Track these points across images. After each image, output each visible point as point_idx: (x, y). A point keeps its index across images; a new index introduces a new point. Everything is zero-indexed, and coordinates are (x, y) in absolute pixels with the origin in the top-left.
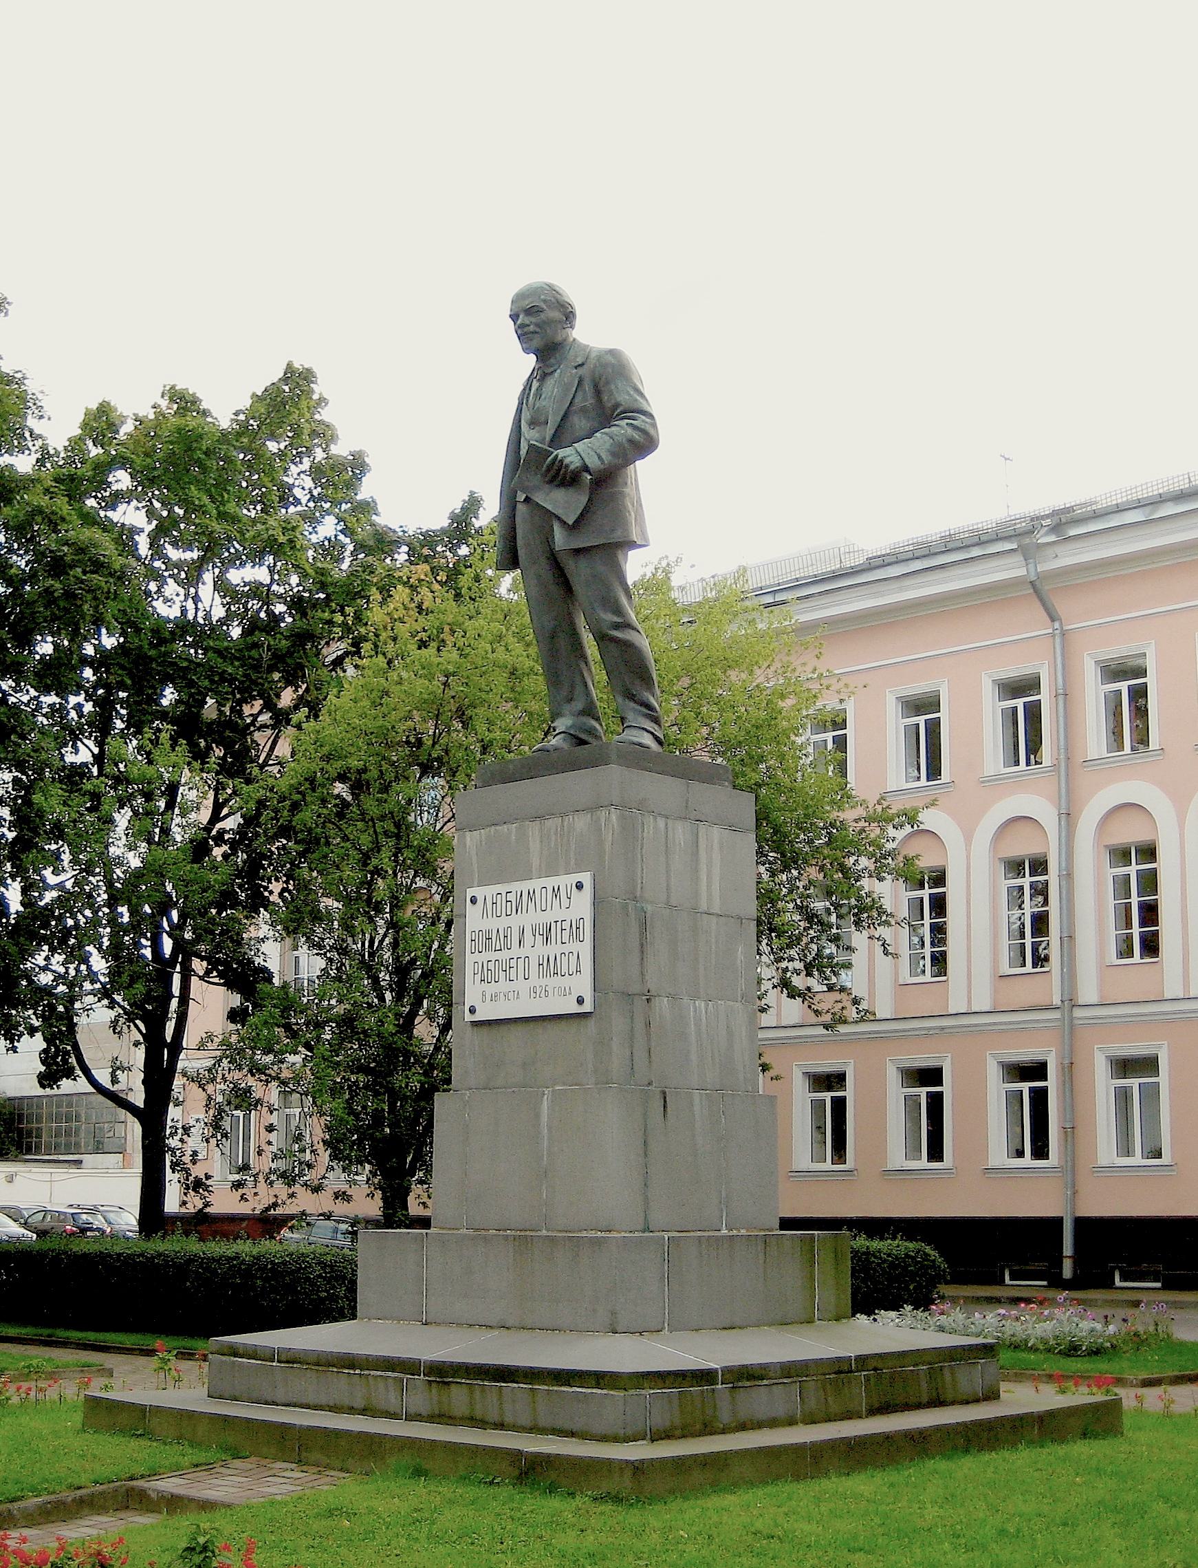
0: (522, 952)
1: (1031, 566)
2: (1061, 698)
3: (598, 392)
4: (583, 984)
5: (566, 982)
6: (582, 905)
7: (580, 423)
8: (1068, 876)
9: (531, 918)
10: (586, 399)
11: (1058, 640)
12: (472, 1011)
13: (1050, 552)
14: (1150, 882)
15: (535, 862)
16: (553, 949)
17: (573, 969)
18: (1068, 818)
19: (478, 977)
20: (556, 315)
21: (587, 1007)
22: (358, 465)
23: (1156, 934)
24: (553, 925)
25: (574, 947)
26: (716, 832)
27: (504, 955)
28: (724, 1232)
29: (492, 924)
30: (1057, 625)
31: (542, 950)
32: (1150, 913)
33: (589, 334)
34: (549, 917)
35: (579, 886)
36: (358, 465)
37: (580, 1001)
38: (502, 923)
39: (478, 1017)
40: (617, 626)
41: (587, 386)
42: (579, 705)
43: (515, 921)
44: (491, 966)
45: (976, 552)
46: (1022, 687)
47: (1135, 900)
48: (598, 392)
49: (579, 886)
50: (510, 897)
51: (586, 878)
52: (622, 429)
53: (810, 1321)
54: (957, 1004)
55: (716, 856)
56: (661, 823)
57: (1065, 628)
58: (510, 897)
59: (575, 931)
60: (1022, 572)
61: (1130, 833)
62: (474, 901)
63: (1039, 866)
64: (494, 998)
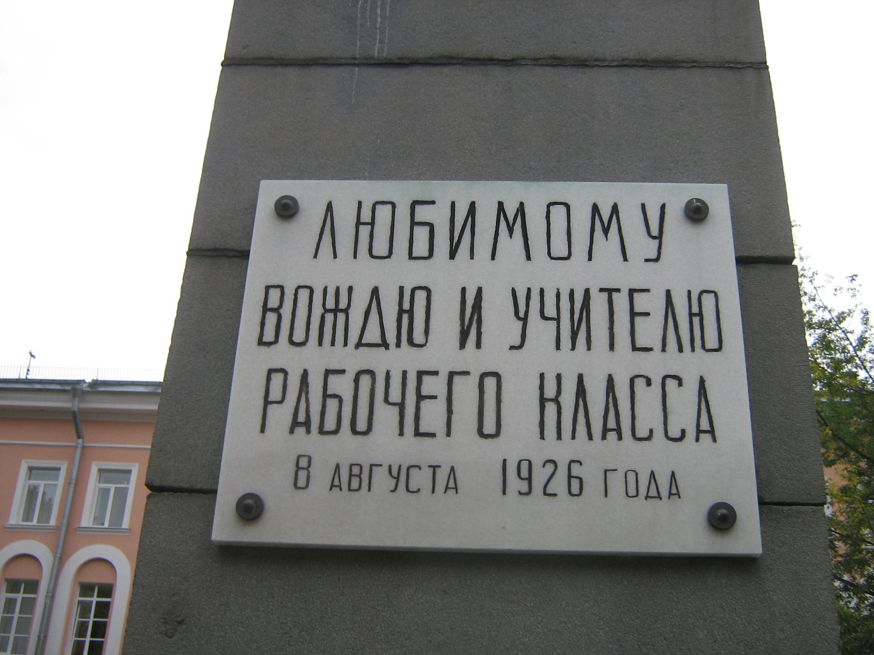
0: (474, 360)
1: (76, 403)
2: (72, 486)
8: (52, 596)
9: (500, 273)
11: (79, 451)
12: (250, 509)
14: (104, 610)
16: (598, 364)
17: (684, 413)
18: (60, 562)
19: (280, 415)
21: (748, 539)
23: (101, 644)
24: (599, 304)
25: (691, 365)
27: (399, 360)
29: (361, 275)
30: (80, 441)
31: (543, 352)
34: (575, 276)
37: (722, 519)
38: (395, 275)
39: (265, 533)
43: (447, 278)
44: (342, 386)
47: (92, 619)
50: (422, 213)
57: (87, 445)
58: (422, 213)
59: (686, 320)
61: (96, 576)
62: (286, 209)
63: (32, 586)
64: (353, 478)
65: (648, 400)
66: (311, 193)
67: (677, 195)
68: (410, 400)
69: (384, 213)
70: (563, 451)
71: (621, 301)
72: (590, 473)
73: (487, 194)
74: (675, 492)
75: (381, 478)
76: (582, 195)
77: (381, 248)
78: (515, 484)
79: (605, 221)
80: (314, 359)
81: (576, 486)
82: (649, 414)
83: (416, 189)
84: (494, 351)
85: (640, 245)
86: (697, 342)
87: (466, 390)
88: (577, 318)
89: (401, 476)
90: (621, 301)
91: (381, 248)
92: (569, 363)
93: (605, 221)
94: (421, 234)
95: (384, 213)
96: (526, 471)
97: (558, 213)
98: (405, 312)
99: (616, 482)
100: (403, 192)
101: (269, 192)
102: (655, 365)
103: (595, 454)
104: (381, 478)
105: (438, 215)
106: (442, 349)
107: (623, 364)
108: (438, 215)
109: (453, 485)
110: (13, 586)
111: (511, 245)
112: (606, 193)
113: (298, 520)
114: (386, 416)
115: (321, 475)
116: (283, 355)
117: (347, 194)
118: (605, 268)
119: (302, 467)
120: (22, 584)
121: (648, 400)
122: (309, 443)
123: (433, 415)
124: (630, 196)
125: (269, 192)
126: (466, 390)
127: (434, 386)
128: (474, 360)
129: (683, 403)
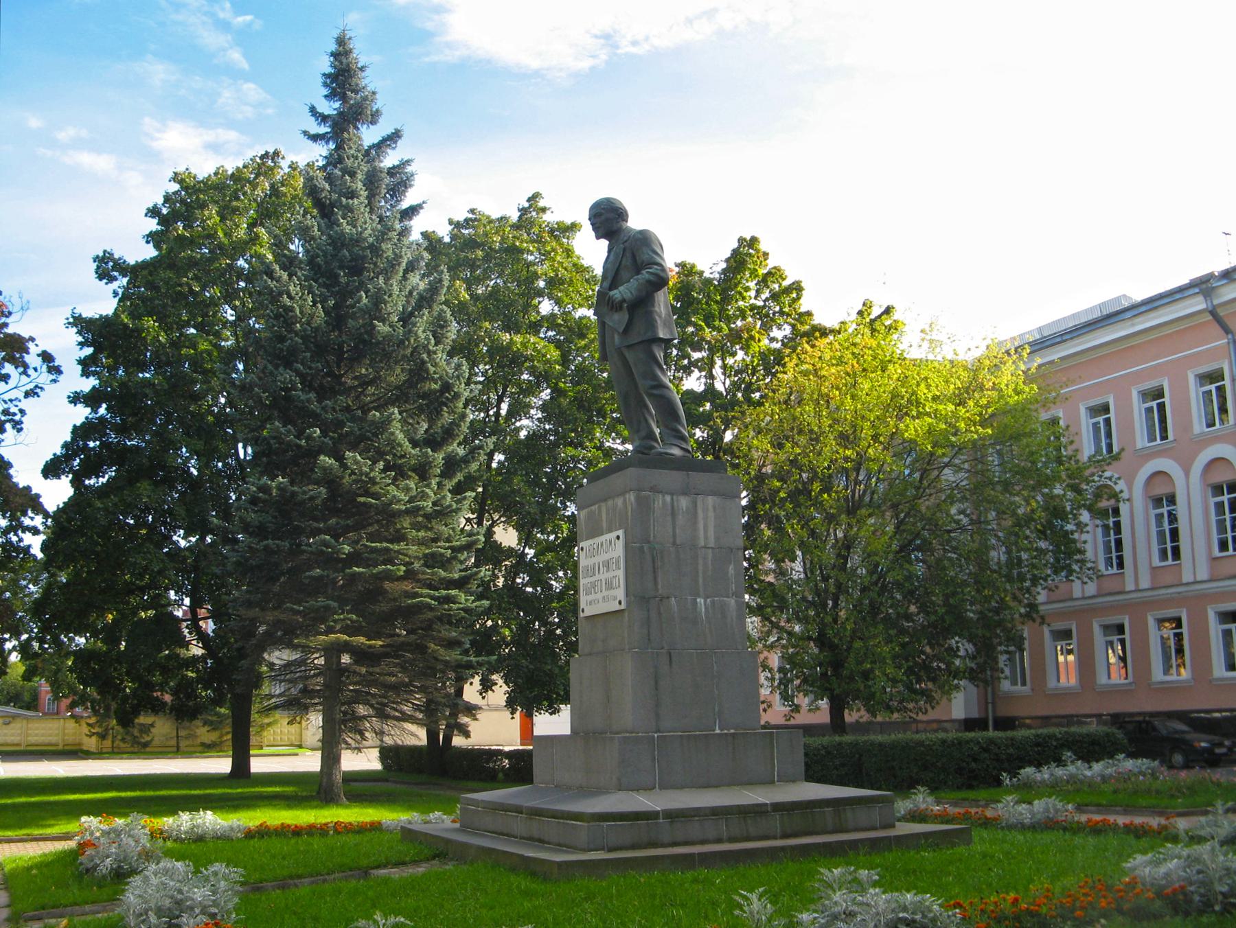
3: (634, 256)
4: (620, 593)
6: (618, 551)
7: (624, 274)
10: (627, 261)
13: (1223, 290)
15: (604, 525)
20: (611, 215)
22: (797, 287)
26: (710, 500)
28: (718, 731)
32: (1175, 534)
33: (635, 222)
35: (618, 538)
36: (797, 287)
40: (654, 387)
41: (628, 254)
42: (643, 433)
45: (1178, 296)
46: (1214, 377)
48: (634, 256)
49: (618, 538)
51: (620, 533)
52: (645, 275)
53: (773, 782)
54: (1187, 577)
55: (711, 514)
56: (668, 498)
60: (1203, 306)
67: (614, 535)
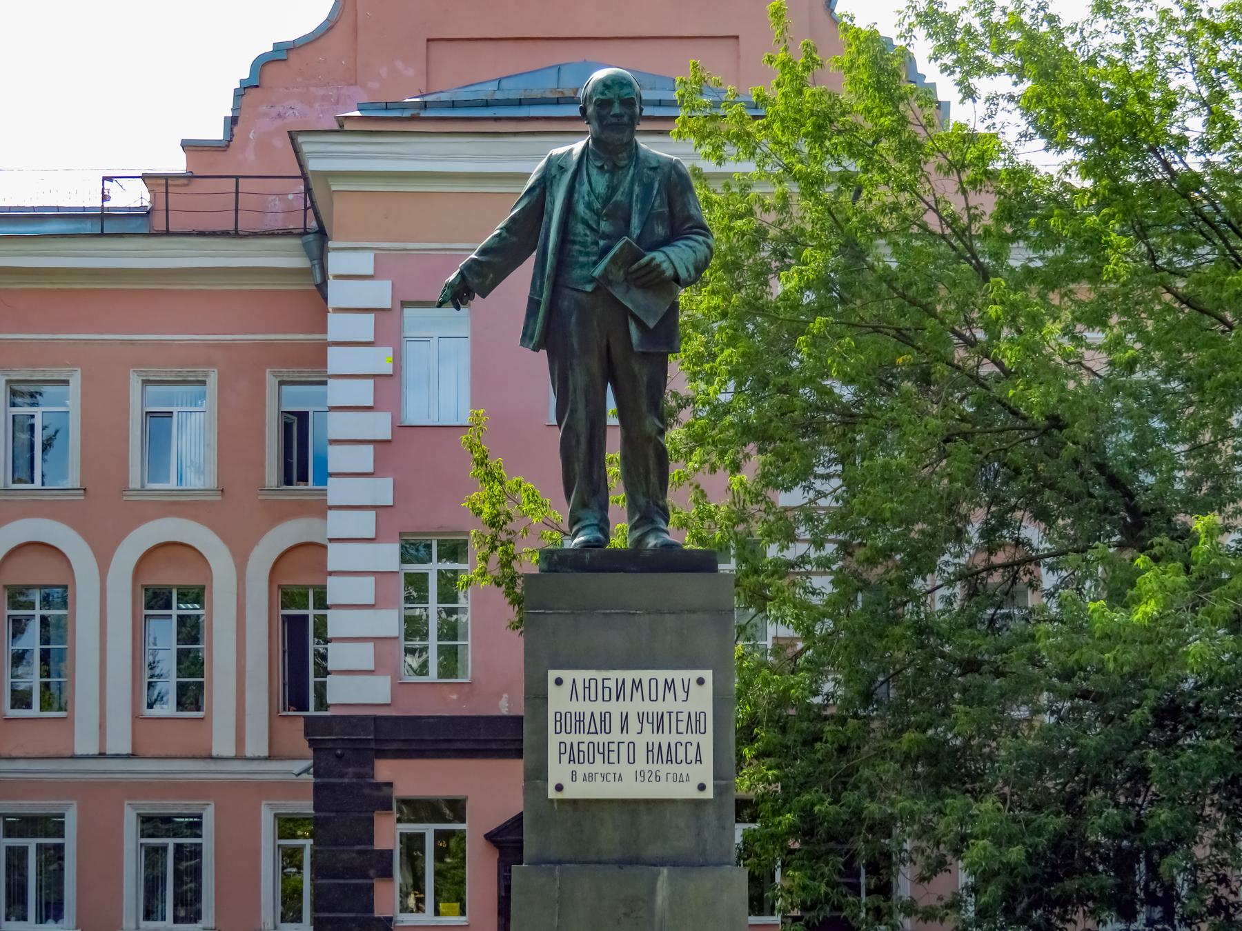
0: (626, 738)
5: (683, 769)
9: (635, 706)
12: (559, 788)
16: (665, 738)
17: (692, 755)
19: (565, 758)
25: (694, 738)
27: (602, 738)
29: (586, 707)
31: (649, 736)
34: (659, 707)
37: (702, 787)
38: (599, 707)
39: (566, 794)
43: (616, 708)
44: (584, 747)
50: (607, 683)
51: (708, 675)
58: (607, 683)
62: (559, 682)
64: (589, 778)
65: (681, 750)
66: (567, 675)
68: (606, 752)
69: (593, 683)
70: (654, 767)
71: (674, 716)
72: (662, 775)
73: (630, 675)
74: (688, 780)
75: (599, 778)
76: (662, 675)
77: (593, 698)
78: (640, 778)
79: (670, 685)
80: (574, 738)
81: (658, 779)
82: (681, 756)
83: (605, 674)
84: (632, 735)
85: (681, 695)
86: (698, 731)
87: (624, 748)
88: (658, 724)
89: (604, 777)
90: (674, 716)
91: (593, 698)
92: (656, 738)
93: (670, 685)
94: (606, 691)
95: (593, 683)
96: (642, 773)
97: (653, 682)
98: (603, 721)
99: (670, 777)
100: (599, 675)
101: (553, 674)
102: (684, 738)
103: (664, 769)
104: (599, 778)
105: (611, 684)
106: (616, 735)
107: (674, 738)
108: (611, 684)
109: (620, 778)
110: (17, 596)
111: (637, 695)
112: (669, 674)
113: (573, 791)
114: (599, 758)
115: (580, 777)
116: (563, 737)
117: (581, 675)
118: (667, 705)
119: (574, 775)
120: (35, 601)
121: (681, 750)
122: (573, 766)
123: (613, 757)
124: (678, 675)
125: (553, 674)
126: (624, 748)
127: (614, 747)
128: (626, 738)
129: (692, 751)
